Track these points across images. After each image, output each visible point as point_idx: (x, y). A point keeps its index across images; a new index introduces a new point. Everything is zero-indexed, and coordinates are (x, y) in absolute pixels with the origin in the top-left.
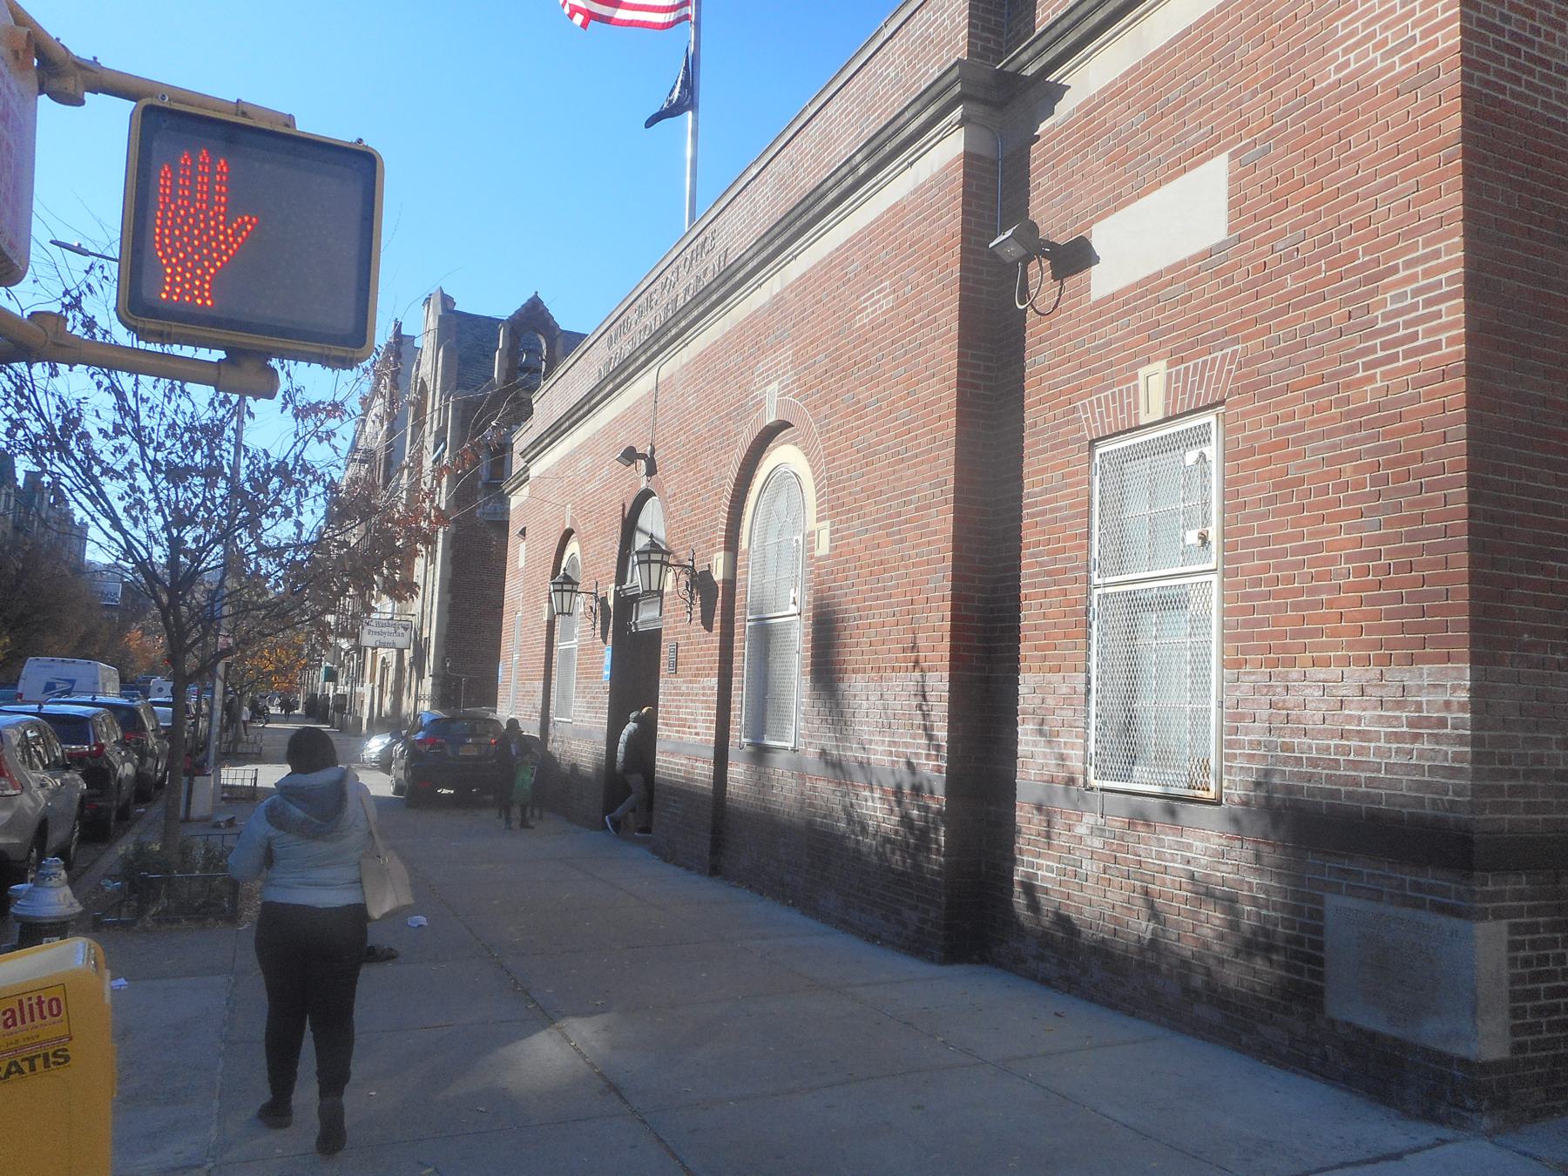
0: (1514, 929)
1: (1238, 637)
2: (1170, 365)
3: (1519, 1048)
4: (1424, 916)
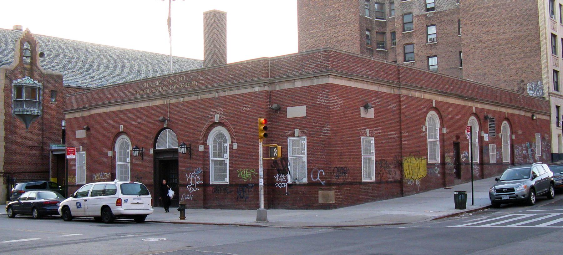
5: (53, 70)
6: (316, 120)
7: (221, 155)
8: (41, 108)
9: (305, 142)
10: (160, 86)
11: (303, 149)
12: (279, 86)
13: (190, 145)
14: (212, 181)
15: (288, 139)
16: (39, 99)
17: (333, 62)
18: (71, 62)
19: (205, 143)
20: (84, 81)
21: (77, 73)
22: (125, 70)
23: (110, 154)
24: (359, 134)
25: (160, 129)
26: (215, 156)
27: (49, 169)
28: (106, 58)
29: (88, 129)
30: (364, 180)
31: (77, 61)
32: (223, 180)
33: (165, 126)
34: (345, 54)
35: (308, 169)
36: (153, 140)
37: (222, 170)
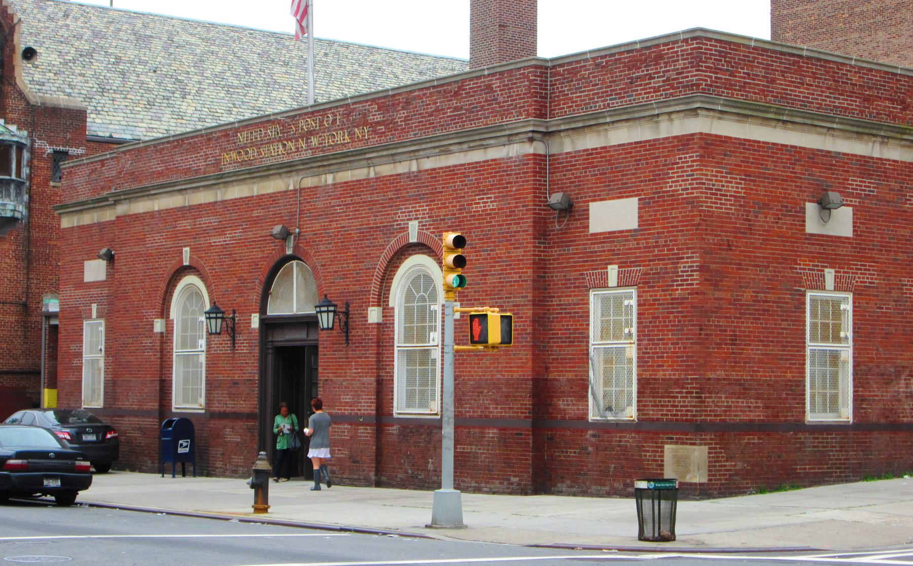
0: (710, 448)
1: (800, 321)
2: (619, 267)
3: (710, 480)
4: (688, 447)
5: (69, 95)
6: (662, 241)
7: (422, 336)
8: (26, 197)
9: (633, 302)
10: (280, 140)
11: (629, 324)
12: (573, 142)
13: (348, 305)
14: (401, 407)
15: (592, 294)
16: (19, 174)
17: (716, 70)
18: (123, 73)
19: (382, 299)
20: (155, 125)
21: (137, 104)
22: (274, 94)
23: (159, 326)
24: (798, 281)
25: (277, 258)
26: (408, 337)
27: (39, 365)
28: (224, 60)
29: (110, 258)
30: (811, 417)
31: (140, 68)
32: (427, 407)
33: (289, 252)
34: (755, 48)
35: (639, 380)
36: (260, 289)
37: (426, 379)
